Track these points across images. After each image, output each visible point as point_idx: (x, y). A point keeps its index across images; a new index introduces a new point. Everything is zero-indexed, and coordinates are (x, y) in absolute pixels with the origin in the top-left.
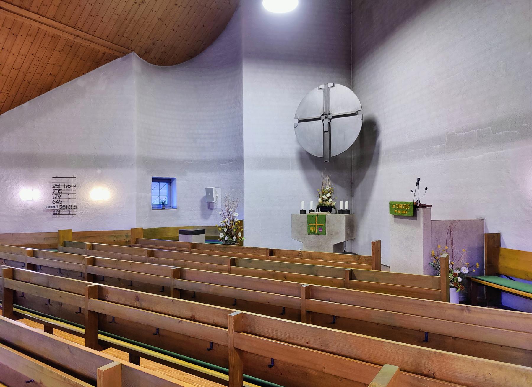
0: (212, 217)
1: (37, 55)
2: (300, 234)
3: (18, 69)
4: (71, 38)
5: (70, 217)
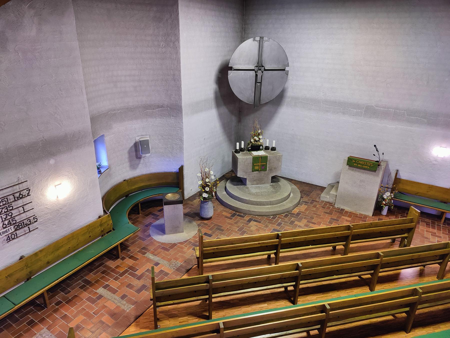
0: (140, 166)
2: (245, 173)
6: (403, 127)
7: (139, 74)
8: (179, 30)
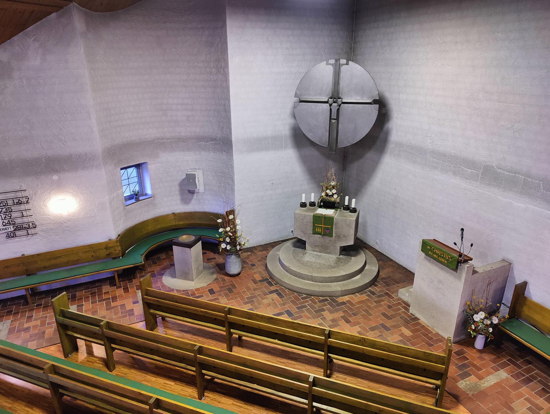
0: (193, 201)
2: (304, 233)
6: (537, 208)
7: (192, 103)
8: (228, 55)
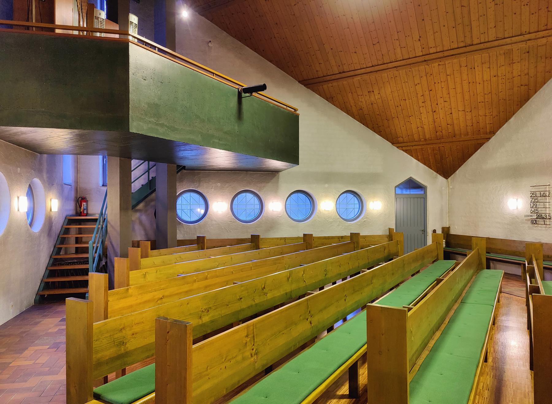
1: (500, 75)
3: (490, 93)
4: (523, 45)
5: (547, 227)
